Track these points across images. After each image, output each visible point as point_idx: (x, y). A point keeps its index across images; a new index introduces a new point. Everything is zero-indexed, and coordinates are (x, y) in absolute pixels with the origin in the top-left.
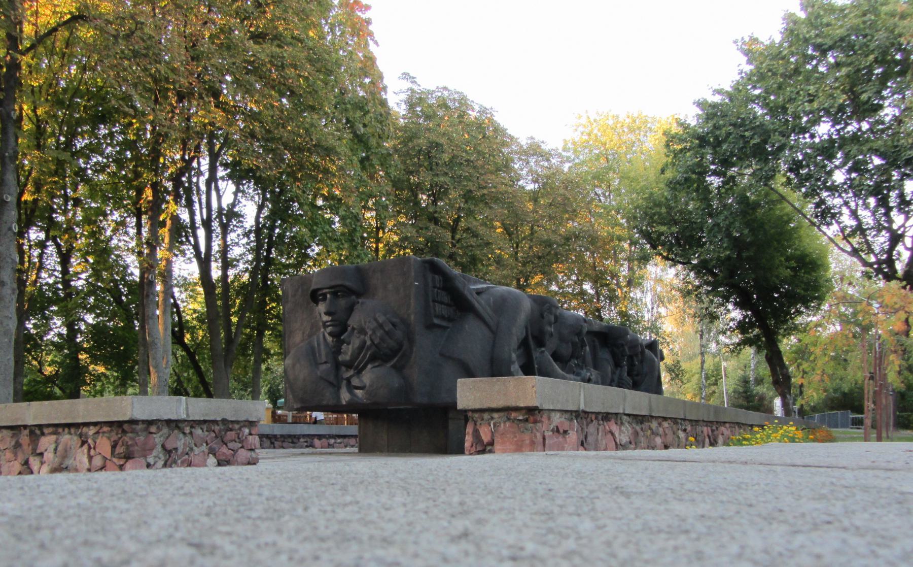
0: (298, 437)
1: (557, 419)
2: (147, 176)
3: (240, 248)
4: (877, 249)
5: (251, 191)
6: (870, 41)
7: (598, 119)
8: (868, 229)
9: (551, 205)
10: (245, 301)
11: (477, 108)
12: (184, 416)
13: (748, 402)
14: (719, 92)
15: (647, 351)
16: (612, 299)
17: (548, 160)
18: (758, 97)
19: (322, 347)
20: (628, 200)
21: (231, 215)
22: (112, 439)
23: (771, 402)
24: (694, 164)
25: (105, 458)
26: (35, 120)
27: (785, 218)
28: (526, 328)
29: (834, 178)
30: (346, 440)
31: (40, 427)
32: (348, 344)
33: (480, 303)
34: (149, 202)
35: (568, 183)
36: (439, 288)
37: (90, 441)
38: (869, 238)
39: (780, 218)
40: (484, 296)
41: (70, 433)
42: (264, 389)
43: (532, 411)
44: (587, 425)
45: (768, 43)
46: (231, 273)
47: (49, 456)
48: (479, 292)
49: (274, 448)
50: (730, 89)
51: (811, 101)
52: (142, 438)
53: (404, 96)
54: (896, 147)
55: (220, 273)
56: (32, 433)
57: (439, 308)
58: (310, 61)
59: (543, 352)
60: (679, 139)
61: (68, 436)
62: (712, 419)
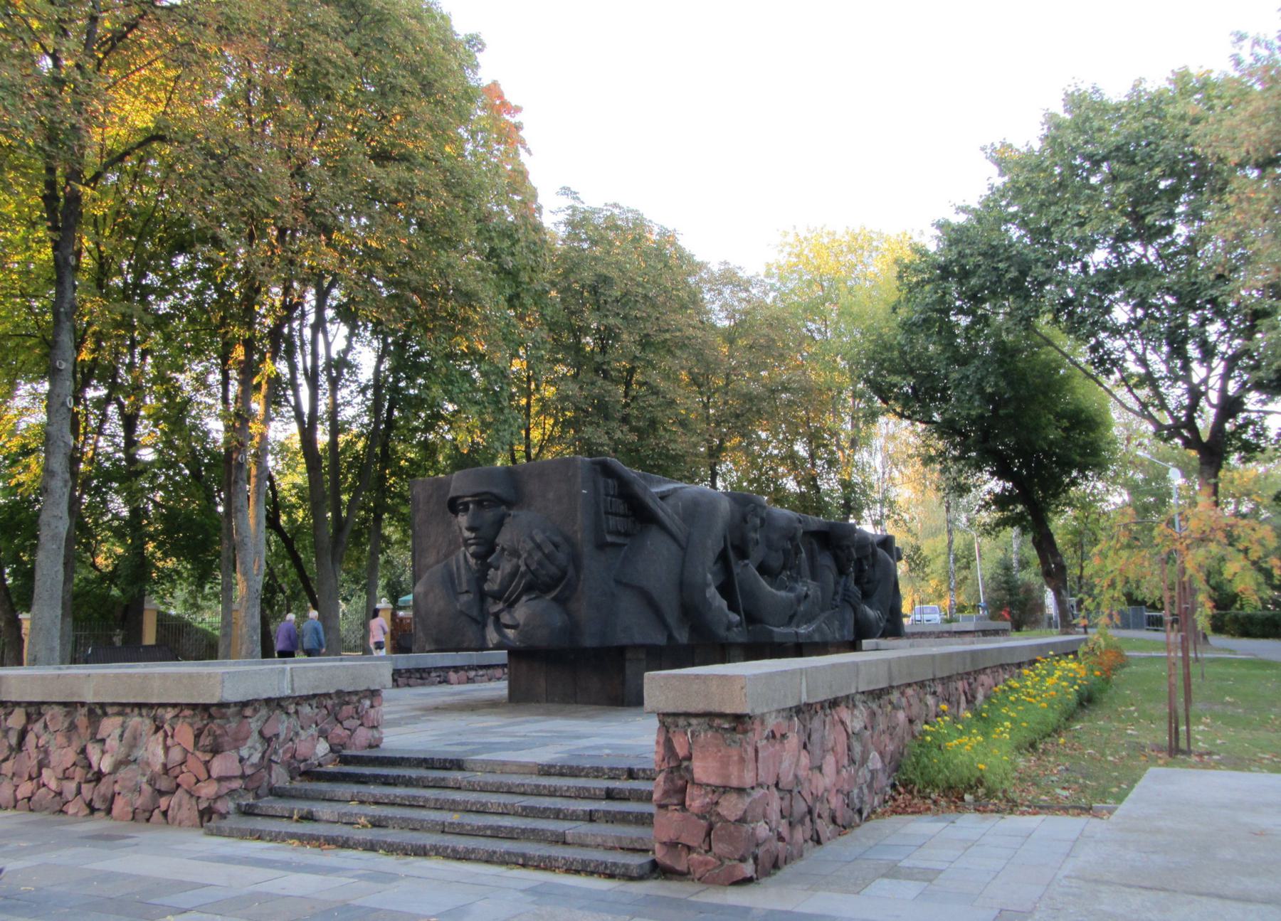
0: (428, 671)
1: (772, 722)
2: (237, 331)
3: (354, 409)
4: (1172, 404)
5: (368, 334)
6: (1155, 150)
7: (809, 236)
8: (1161, 378)
9: (751, 347)
10: (358, 476)
11: (656, 230)
12: (288, 692)
13: (1011, 595)
14: (964, 210)
15: (880, 550)
16: (832, 463)
17: (747, 290)
18: (1014, 215)
19: (463, 571)
20: (852, 338)
21: (340, 365)
22: (196, 726)
23: (1042, 598)
24: (934, 302)
25: (186, 751)
26: (97, 256)
27: (1054, 365)
28: (725, 538)
29: (1114, 315)
30: (490, 672)
31: (102, 705)
32: (497, 569)
33: (665, 512)
35: (776, 322)
36: (613, 496)
37: (167, 727)
38: (1162, 390)
39: (1046, 364)
40: (671, 501)
41: (141, 715)
42: (382, 582)
43: (739, 719)
44: (811, 719)
45: (1024, 150)
46: (342, 438)
47: (112, 743)
48: (663, 497)
49: (398, 686)
50: (978, 206)
51: (1081, 225)
52: (234, 725)
53: (563, 217)
54: (1194, 283)
55: (327, 438)
56: (91, 712)
57: (613, 521)
58: (447, 185)
59: (746, 565)
60: (915, 270)
61: (138, 719)
62: (968, 670)
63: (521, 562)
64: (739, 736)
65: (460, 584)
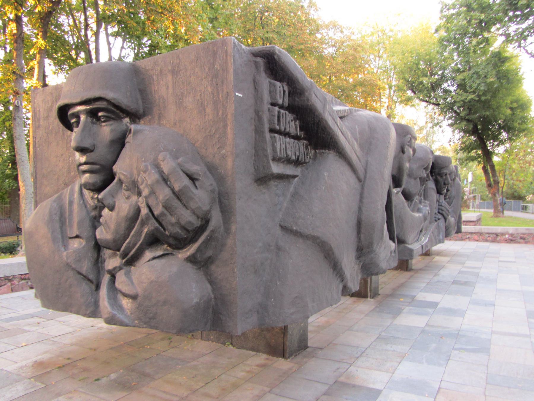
19: (76, 207)
34: (14, 35)
36: (281, 107)
57: (281, 142)
63: (142, 203)
65: (71, 227)
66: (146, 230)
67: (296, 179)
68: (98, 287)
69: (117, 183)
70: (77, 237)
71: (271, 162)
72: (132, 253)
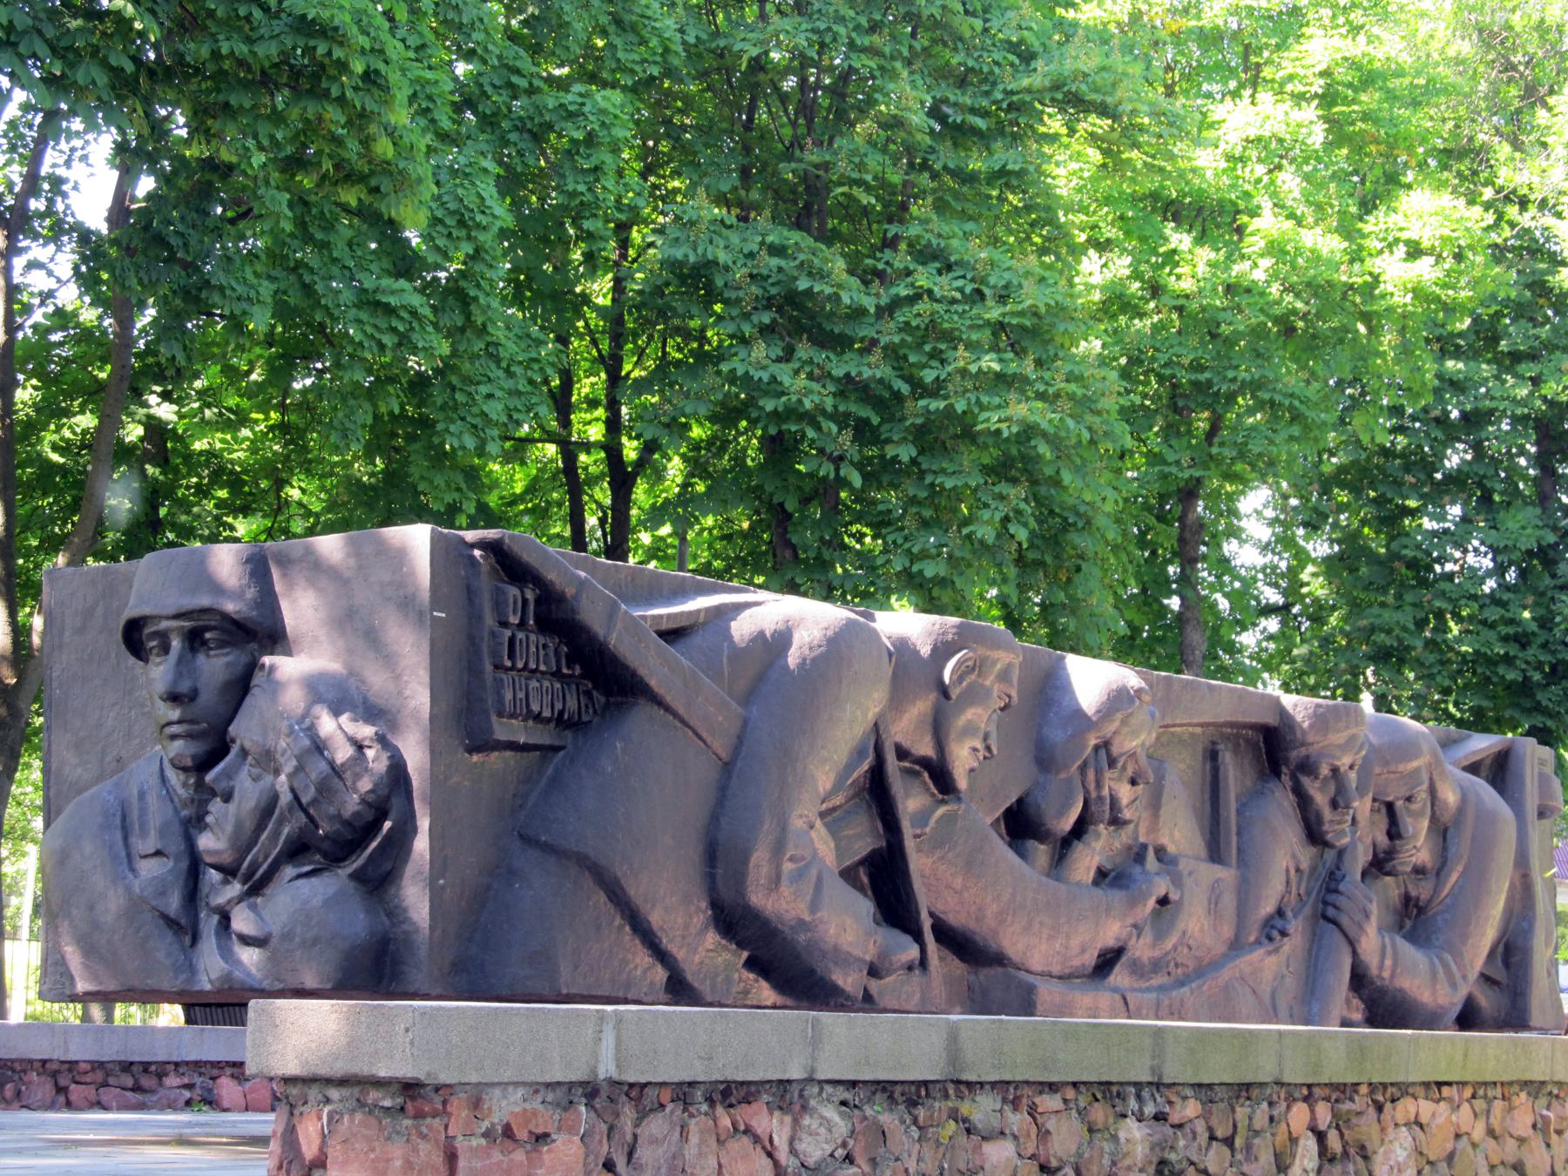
1: (504, 1107)
19: (153, 800)
48: (673, 634)
49: (69, 1105)
64: (408, 1122)
66: (286, 831)
67: (561, 753)
68: (195, 939)
69: (237, 755)
70: (158, 853)
71: (494, 718)
72: (261, 871)
